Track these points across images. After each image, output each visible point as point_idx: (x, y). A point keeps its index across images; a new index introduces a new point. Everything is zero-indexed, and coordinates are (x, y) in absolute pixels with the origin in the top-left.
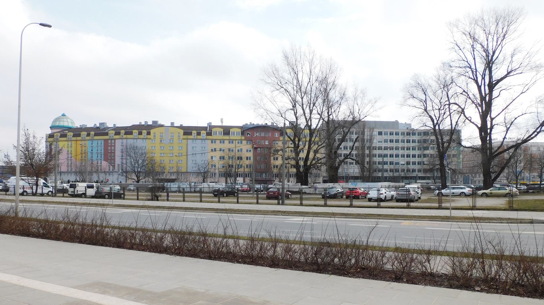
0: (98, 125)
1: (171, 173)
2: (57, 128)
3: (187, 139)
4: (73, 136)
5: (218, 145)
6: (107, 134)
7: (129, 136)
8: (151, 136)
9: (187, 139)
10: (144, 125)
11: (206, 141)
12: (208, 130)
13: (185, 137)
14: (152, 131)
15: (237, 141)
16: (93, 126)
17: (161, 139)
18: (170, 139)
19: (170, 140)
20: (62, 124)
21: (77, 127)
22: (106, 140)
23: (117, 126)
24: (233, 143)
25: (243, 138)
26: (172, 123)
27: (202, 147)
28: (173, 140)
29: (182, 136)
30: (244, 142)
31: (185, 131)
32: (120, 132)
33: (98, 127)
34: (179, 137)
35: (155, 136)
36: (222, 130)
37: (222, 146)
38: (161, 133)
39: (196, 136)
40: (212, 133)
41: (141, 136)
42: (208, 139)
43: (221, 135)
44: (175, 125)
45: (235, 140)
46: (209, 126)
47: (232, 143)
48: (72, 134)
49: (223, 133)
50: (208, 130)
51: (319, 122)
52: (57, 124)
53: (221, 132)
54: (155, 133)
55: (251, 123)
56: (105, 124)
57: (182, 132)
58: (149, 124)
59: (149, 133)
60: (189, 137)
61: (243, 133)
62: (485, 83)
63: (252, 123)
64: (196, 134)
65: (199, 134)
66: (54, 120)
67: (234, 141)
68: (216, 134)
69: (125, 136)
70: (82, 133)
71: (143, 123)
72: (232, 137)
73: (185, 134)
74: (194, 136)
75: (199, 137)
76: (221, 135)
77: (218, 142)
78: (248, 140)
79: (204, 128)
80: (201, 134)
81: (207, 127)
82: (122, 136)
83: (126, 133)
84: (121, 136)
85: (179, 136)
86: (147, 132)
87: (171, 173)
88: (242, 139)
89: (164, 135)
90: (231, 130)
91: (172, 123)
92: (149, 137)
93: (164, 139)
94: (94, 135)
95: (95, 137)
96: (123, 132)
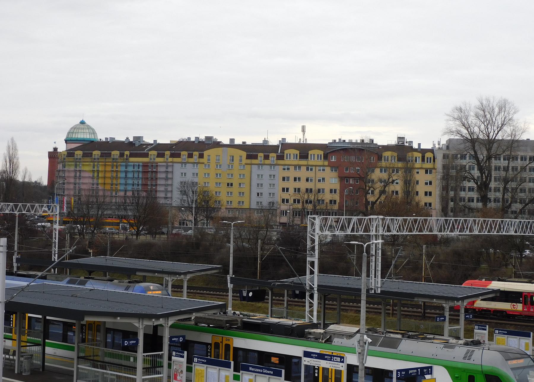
0: (131, 140)
1: (229, 209)
2: (75, 142)
3: (251, 164)
4: (157, 157)
5: (292, 173)
6: (146, 155)
7: (176, 160)
8: (204, 160)
9: (251, 164)
10: (194, 142)
11: (276, 167)
12: (279, 152)
13: (249, 161)
14: (206, 153)
15: (318, 168)
16: (124, 140)
17: (233, 162)
18: (228, 164)
19: (229, 166)
20: (80, 136)
21: (101, 139)
22: (145, 165)
23: (158, 142)
24: (427, 158)
25: (326, 163)
26: (232, 140)
27: (217, 183)
28: (232, 166)
29: (245, 161)
30: (328, 169)
31: (248, 153)
32: (180, 154)
33: (132, 142)
34: (240, 162)
35: (209, 160)
36: (297, 152)
37: (297, 174)
38: (217, 156)
39: (263, 161)
40: (284, 155)
41: (191, 160)
42: (279, 165)
43: (297, 158)
44: (237, 142)
45: (316, 166)
46: (282, 144)
47: (311, 170)
48: (155, 153)
49: (299, 155)
50: (279, 152)
51: (72, 136)
52: (75, 136)
53: (321, 155)
54: (209, 156)
55: (155, 141)
56: (141, 138)
57: (244, 154)
58: (358, 142)
59: (201, 156)
60: (254, 161)
61: (326, 157)
62: (419, 292)
63: (343, 139)
64: (263, 158)
65: (266, 157)
66: (74, 126)
67: (314, 168)
68: (290, 158)
69: (170, 159)
70: (113, 153)
71: (193, 139)
72: (311, 162)
73: (249, 157)
74: (261, 161)
75: (267, 162)
76: (297, 158)
77: (292, 168)
78: (334, 167)
79: (274, 148)
80: (270, 158)
81: (279, 146)
82: (167, 159)
83: (172, 156)
84: (165, 159)
85: (241, 160)
86: (199, 154)
87: (229, 209)
88: (325, 164)
89: (221, 158)
90: (310, 152)
91: (232, 140)
92: (201, 160)
93: (221, 164)
94: (157, 156)
95: (130, 158)
96: (168, 153)
